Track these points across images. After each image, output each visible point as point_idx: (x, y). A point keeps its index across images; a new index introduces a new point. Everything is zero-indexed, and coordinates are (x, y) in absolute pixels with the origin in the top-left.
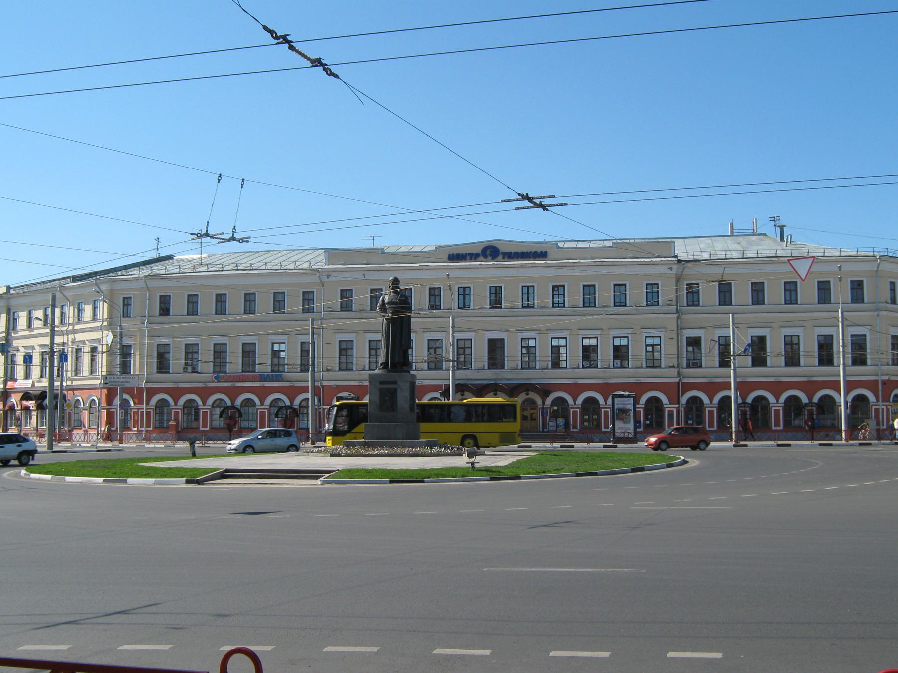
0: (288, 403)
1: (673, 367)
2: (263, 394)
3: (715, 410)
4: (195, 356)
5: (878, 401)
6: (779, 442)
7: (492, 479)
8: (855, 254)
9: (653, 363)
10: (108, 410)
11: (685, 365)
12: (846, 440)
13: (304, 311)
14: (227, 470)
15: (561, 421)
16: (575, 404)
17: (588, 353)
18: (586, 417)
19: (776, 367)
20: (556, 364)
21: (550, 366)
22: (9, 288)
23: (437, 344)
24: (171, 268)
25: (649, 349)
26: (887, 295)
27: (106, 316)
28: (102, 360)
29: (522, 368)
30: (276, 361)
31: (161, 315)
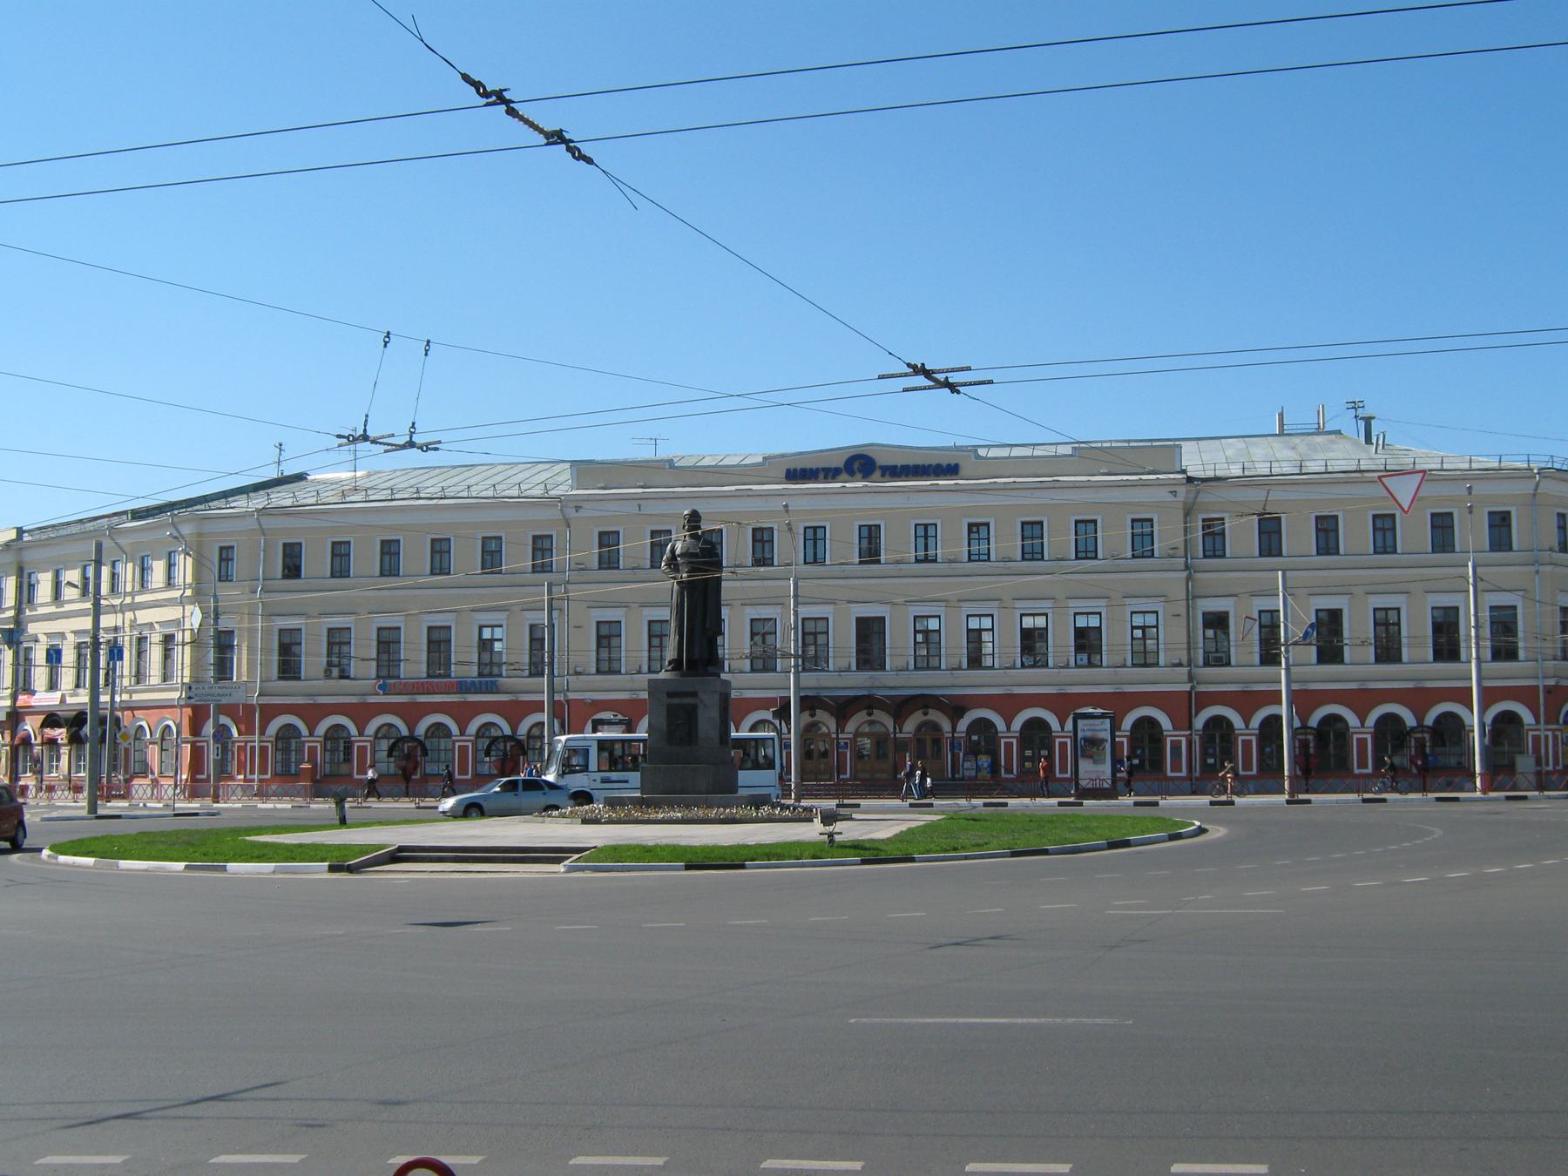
0: (507, 731)
1: (1180, 665)
2: (463, 714)
3: (1254, 739)
4: (345, 649)
5: (1538, 721)
6: (1366, 796)
8: (1496, 465)
9: (1144, 659)
10: (193, 744)
11: (1201, 662)
12: (1484, 791)
13: (535, 569)
14: (401, 849)
15: (984, 760)
16: (1009, 730)
17: (1032, 641)
18: (1028, 753)
19: (1359, 665)
20: (975, 660)
21: (965, 665)
22: (20, 531)
23: (821, 625)
24: (304, 496)
25: (1138, 633)
27: (189, 580)
28: (183, 656)
29: (916, 668)
30: (486, 657)
31: (285, 577)
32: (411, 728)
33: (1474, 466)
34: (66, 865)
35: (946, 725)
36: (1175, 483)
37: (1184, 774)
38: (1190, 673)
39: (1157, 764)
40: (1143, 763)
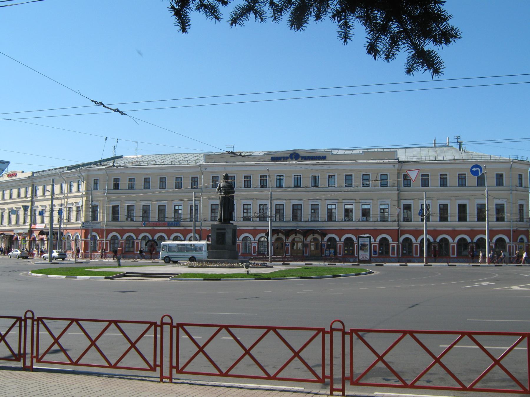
1: (395, 221)
4: (132, 212)
5: (510, 241)
6: (450, 264)
7: (256, 279)
8: (499, 158)
9: (383, 219)
10: (85, 241)
11: (402, 220)
14: (127, 273)
15: (332, 250)
16: (340, 241)
17: (348, 212)
18: (346, 248)
19: (453, 222)
21: (327, 220)
22: (33, 173)
26: (517, 182)
27: (84, 189)
28: (82, 214)
29: (311, 221)
30: (177, 215)
32: (153, 237)
33: (492, 159)
34: (34, 276)
35: (320, 238)
36: (394, 163)
37: (396, 256)
38: (398, 224)
39: (387, 253)
40: (383, 252)
